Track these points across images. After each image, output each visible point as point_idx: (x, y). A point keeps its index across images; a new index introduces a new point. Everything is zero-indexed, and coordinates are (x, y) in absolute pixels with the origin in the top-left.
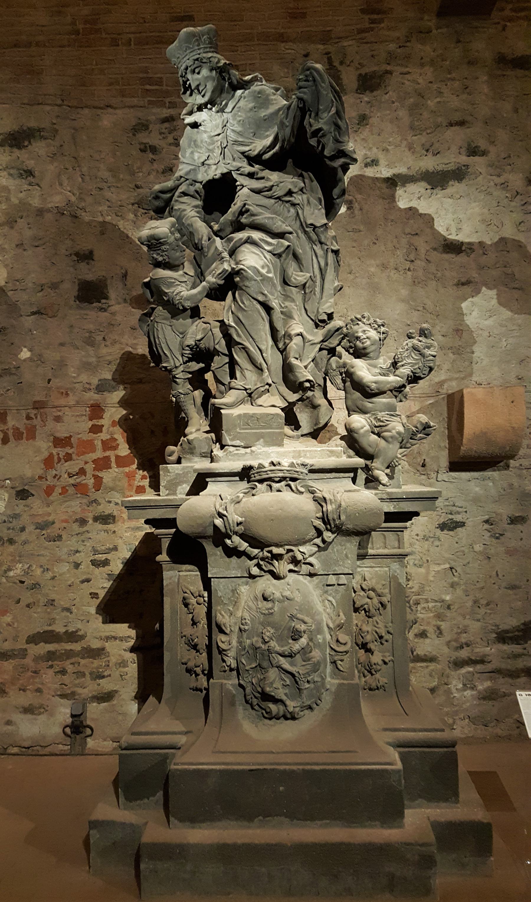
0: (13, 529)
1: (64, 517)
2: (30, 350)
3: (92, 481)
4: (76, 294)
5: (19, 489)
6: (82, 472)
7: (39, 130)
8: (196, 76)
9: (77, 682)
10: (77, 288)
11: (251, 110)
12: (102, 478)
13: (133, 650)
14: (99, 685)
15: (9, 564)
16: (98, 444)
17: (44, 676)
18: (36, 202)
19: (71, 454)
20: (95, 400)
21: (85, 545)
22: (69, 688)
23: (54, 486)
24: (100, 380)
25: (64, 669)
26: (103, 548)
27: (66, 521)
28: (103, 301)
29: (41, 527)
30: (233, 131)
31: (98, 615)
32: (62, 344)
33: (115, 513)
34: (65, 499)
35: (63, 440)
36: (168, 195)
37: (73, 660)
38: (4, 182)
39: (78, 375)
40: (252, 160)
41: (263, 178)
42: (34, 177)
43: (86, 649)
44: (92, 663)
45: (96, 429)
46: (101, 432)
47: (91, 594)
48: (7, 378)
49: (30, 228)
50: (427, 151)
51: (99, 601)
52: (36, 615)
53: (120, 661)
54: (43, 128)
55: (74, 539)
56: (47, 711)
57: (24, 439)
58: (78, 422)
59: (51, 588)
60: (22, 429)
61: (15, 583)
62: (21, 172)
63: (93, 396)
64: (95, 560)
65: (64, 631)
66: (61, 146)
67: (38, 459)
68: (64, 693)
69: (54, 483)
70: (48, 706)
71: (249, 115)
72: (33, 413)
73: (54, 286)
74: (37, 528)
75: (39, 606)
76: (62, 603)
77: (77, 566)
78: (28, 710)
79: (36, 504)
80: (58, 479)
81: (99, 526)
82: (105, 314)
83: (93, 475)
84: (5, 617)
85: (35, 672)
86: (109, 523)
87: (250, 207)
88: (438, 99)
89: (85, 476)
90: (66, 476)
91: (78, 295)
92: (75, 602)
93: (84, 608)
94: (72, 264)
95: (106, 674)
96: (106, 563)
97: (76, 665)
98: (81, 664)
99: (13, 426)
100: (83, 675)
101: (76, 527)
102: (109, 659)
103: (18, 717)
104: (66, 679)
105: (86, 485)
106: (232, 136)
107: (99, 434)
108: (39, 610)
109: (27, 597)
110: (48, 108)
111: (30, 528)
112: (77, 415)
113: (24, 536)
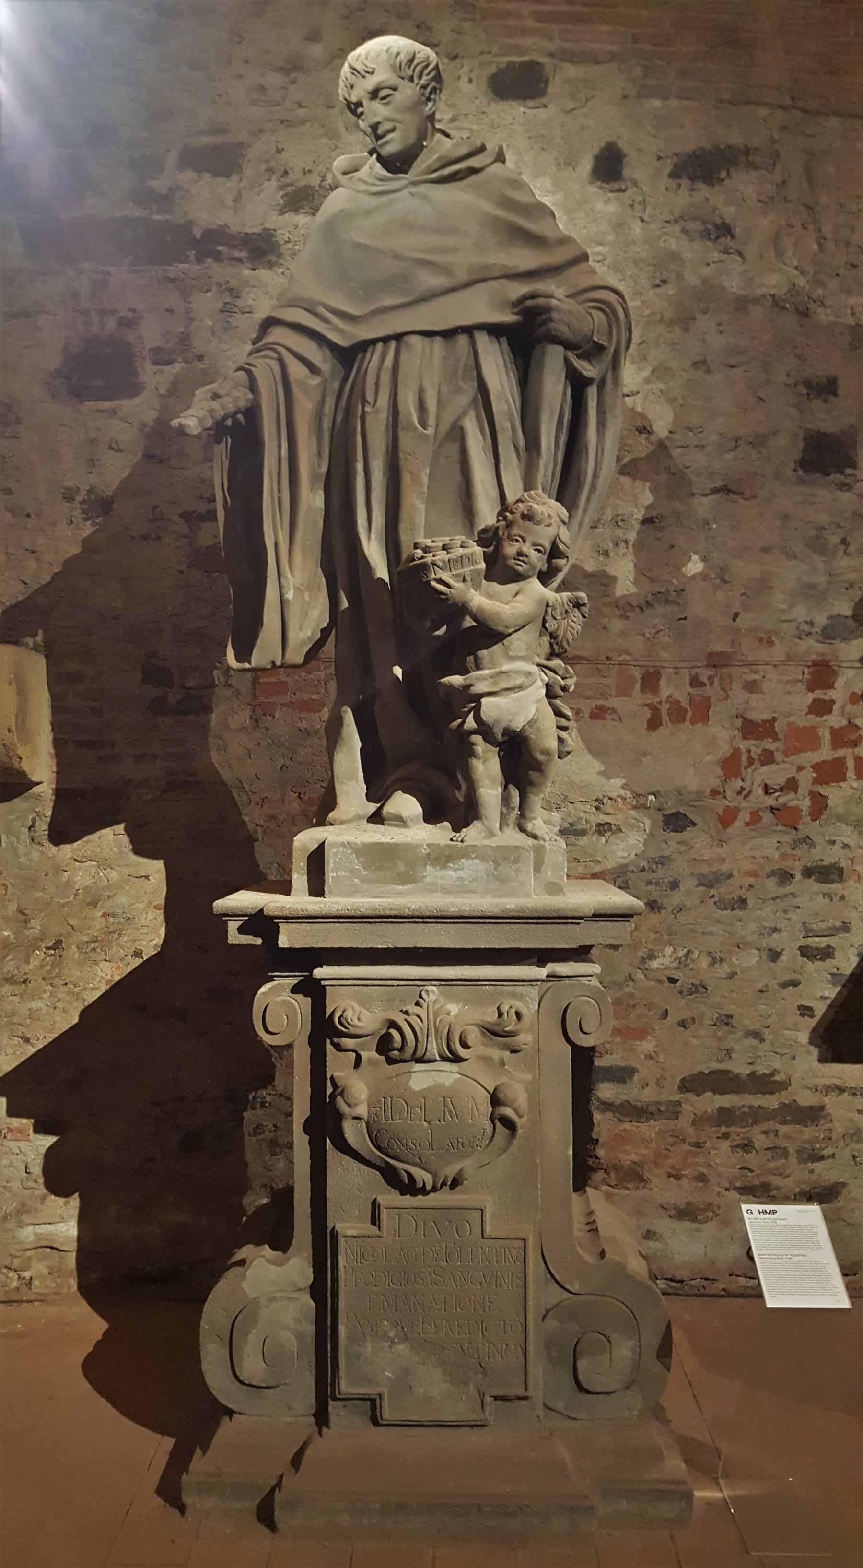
0: (657, 884)
1: (748, 866)
2: (704, 559)
3: (807, 802)
4: (797, 455)
5: (668, 812)
6: (791, 785)
7: (747, 151)
9: (771, 1165)
10: (801, 445)
12: (826, 798)
14: (812, 1172)
15: (650, 946)
16: (826, 736)
17: (713, 1152)
18: (733, 285)
19: (772, 752)
20: (818, 654)
21: (789, 919)
22: (758, 1176)
23: (737, 810)
24: (829, 618)
25: (750, 1141)
26: (823, 926)
27: (754, 874)
28: (849, 471)
29: (709, 882)
31: (812, 1047)
32: (766, 550)
33: (843, 864)
34: (754, 834)
35: (758, 725)
37: (765, 1126)
39: (791, 607)
42: (733, 237)
43: (788, 1106)
44: (801, 1132)
45: (822, 708)
46: (830, 711)
47: (799, 1008)
48: (660, 609)
51: (813, 1022)
52: (695, 1041)
53: (852, 1132)
54: (756, 149)
55: (768, 909)
56: (717, 1215)
57: (687, 723)
58: (789, 692)
59: (726, 994)
60: (685, 703)
61: (659, 981)
62: (709, 226)
63: (813, 648)
64: (807, 947)
65: (748, 1072)
66: (784, 182)
67: (709, 758)
68: (748, 1184)
69: (736, 804)
70: (719, 1208)
72: (705, 674)
73: (759, 441)
74: (700, 884)
75: (702, 1025)
76: (747, 1022)
77: (774, 955)
78: (686, 1213)
79: (699, 840)
80: (745, 797)
81: (813, 885)
83: (811, 793)
84: (644, 1043)
85: (698, 1145)
86: (832, 882)
89: (796, 793)
90: (760, 792)
91: (803, 458)
92: (769, 1021)
93: (786, 1032)
95: (825, 1153)
96: (827, 953)
97: (771, 1136)
98: (780, 1133)
99: (669, 697)
100: (784, 1153)
101: (771, 885)
102: (830, 1126)
103: (664, 1225)
104: (751, 1159)
105: (797, 810)
107: (825, 718)
108: (702, 1033)
109: (679, 1008)
110: (763, 112)
111: (688, 884)
112: (789, 681)
113: (675, 899)
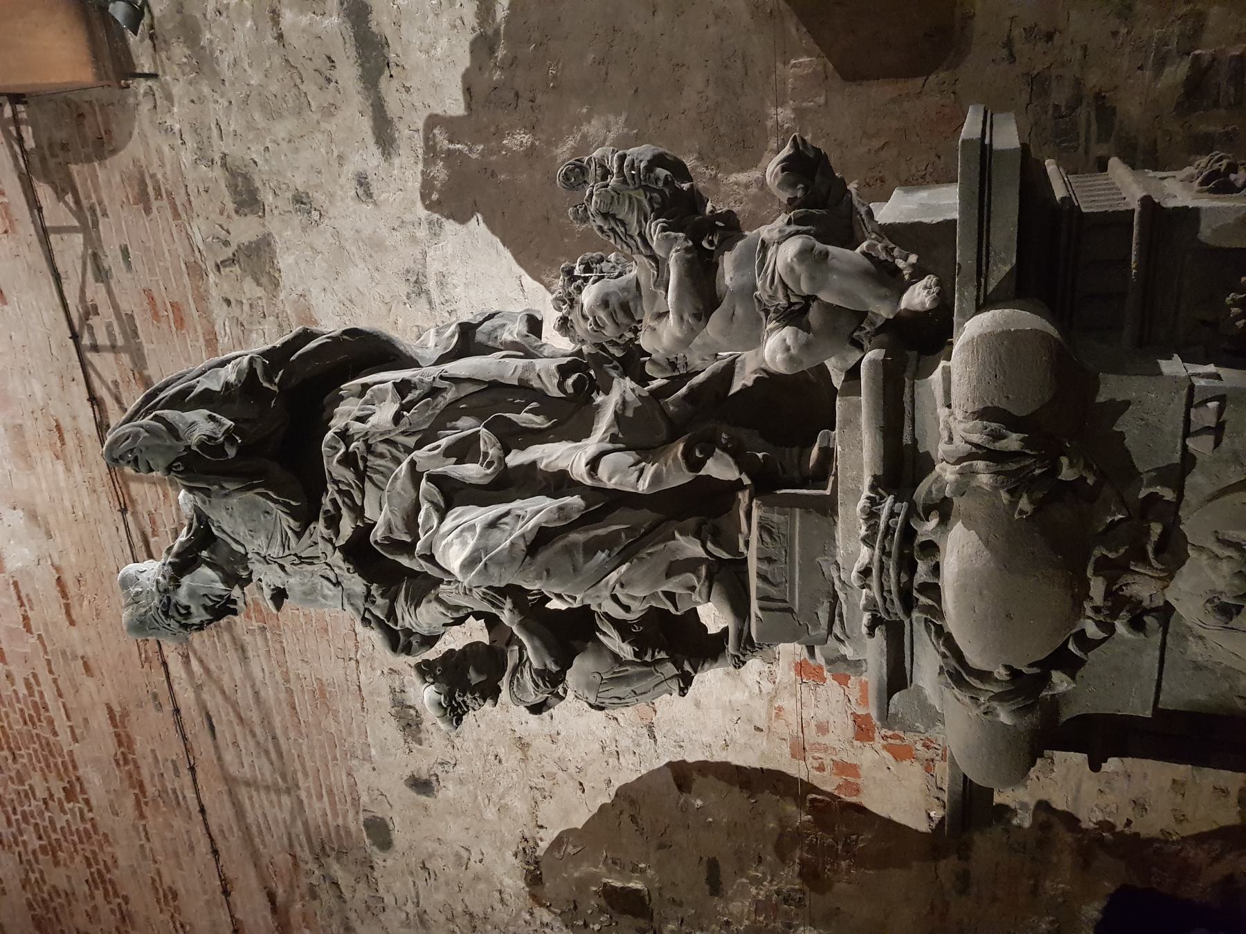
50: (329, 80)
71: (239, 520)
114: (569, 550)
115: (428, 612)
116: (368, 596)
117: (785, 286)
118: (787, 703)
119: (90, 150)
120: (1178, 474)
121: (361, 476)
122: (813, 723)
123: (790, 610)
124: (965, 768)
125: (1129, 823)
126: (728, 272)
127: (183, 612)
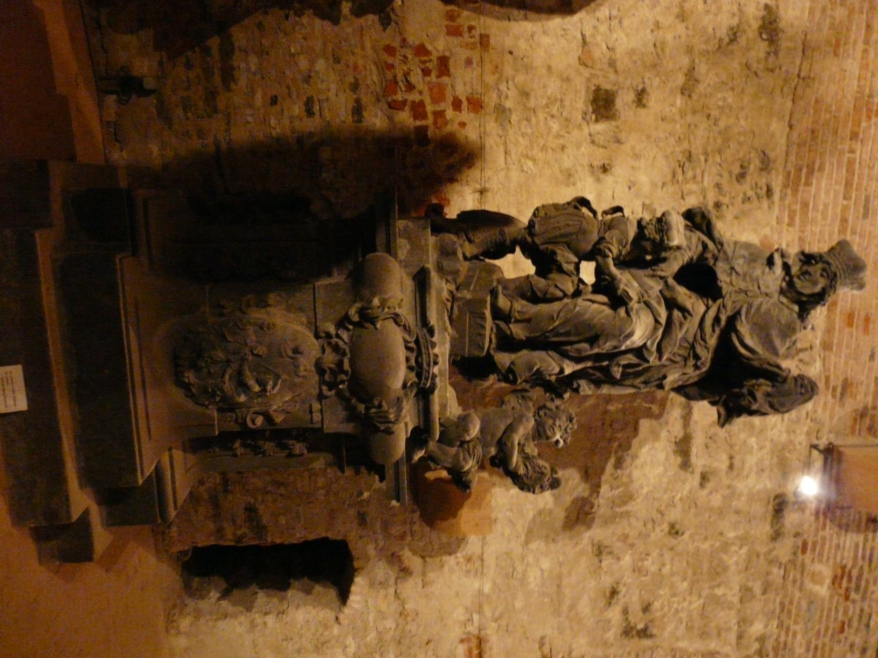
3: (400, 99)
6: (410, 87)
8: (819, 273)
11: (779, 321)
13: (217, 144)
28: (594, 117)
30: (761, 304)
36: (705, 229)
38: (726, 8)
40: (732, 320)
41: (714, 331)
45: (457, 105)
49: (675, 38)
50: (711, 438)
58: (465, 85)
71: (775, 318)
73: (612, 64)
81: (351, 104)
82: (580, 117)
87: (688, 321)
88: (755, 447)
94: (634, 85)
105: (395, 93)
106: (757, 302)
114: (578, 334)
115: (704, 192)
116: (716, 259)
117: (469, 454)
118: (490, 79)
119: (870, 412)
120: (321, 397)
121: (693, 347)
122: (475, 65)
123: (471, 313)
124: (391, 258)
125: (287, 17)
126: (493, 451)
127: (825, 274)
